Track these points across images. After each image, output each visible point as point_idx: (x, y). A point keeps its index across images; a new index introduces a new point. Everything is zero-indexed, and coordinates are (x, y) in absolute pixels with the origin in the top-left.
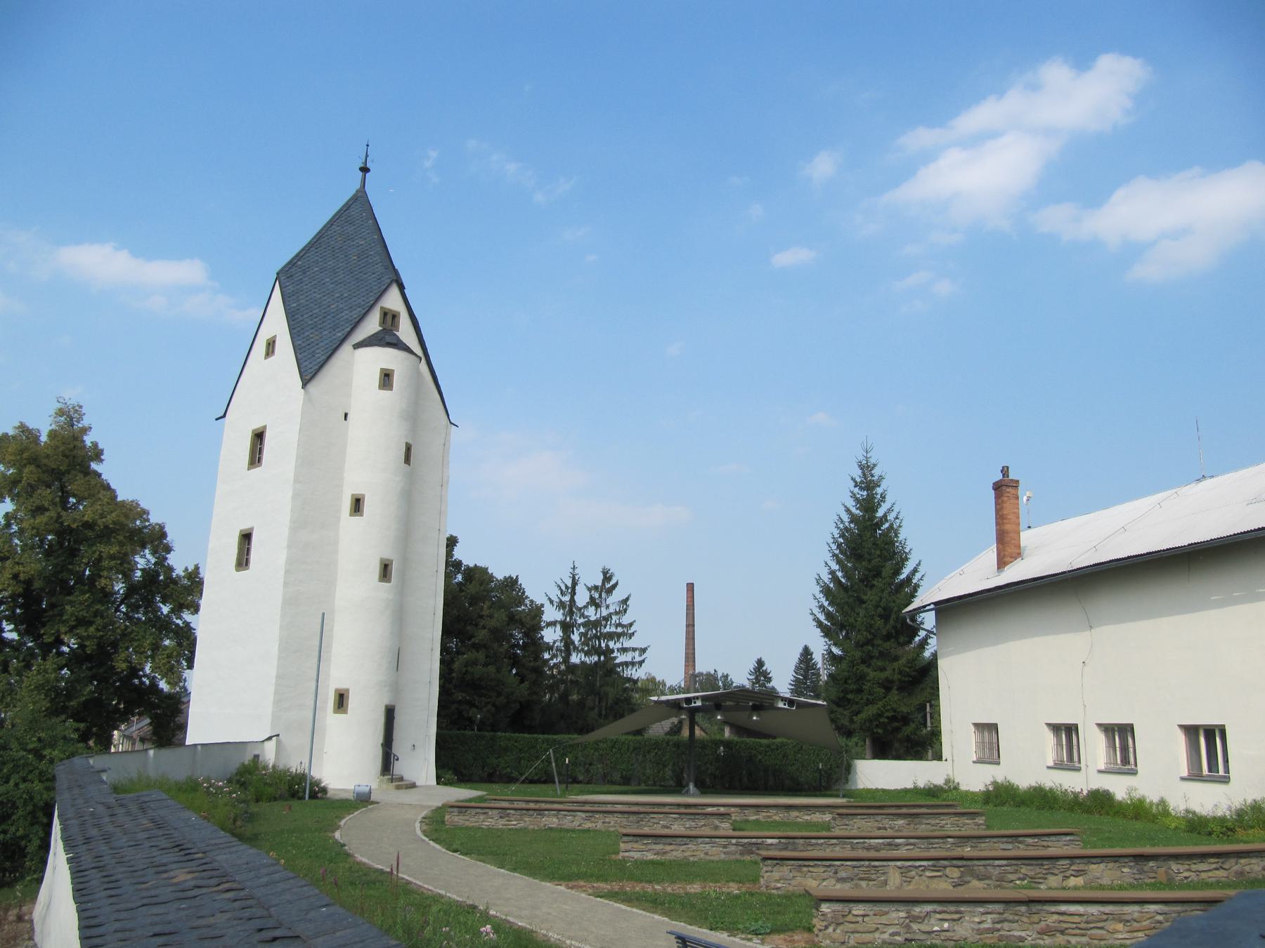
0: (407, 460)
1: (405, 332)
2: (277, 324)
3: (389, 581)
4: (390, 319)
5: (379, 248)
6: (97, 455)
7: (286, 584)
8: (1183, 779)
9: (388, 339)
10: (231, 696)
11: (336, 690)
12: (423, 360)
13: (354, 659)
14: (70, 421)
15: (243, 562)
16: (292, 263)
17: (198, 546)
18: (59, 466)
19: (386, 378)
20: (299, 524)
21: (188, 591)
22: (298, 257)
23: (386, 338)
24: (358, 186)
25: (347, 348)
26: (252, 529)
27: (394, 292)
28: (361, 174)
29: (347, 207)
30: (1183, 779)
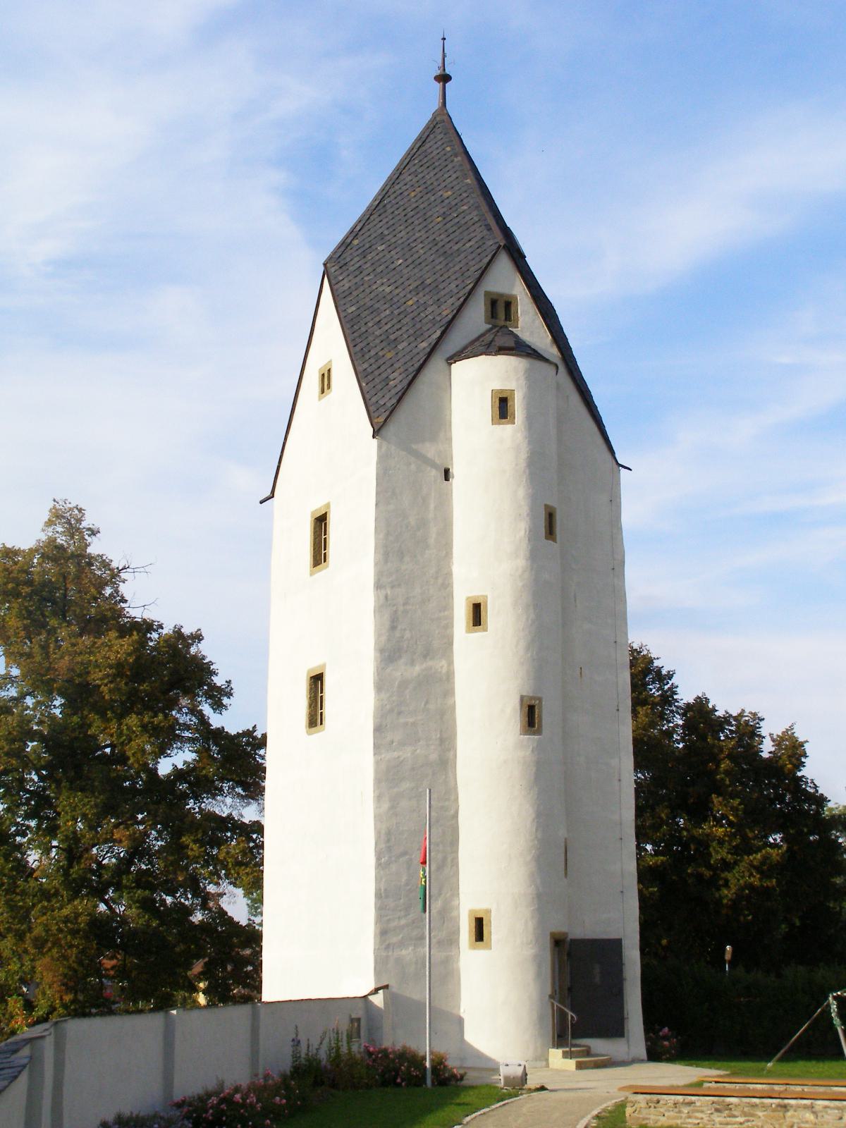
0: (550, 531)
1: (529, 325)
2: (332, 344)
3: (539, 732)
4: (501, 308)
5: (477, 198)
6: (793, 750)
7: (377, 747)
8: (807, 741)
9: (503, 341)
10: (316, 938)
11: (489, 947)
12: (562, 369)
13: (491, 865)
14: (69, 520)
15: (315, 719)
16: (345, 245)
17: (261, 700)
18: (60, 589)
19: (503, 407)
20: (389, 654)
21: (241, 761)
22: (354, 233)
23: (499, 338)
24: (435, 105)
25: (437, 362)
26: (324, 666)
27: (504, 264)
28: (438, 86)
29: (422, 140)
30: (807, 741)
